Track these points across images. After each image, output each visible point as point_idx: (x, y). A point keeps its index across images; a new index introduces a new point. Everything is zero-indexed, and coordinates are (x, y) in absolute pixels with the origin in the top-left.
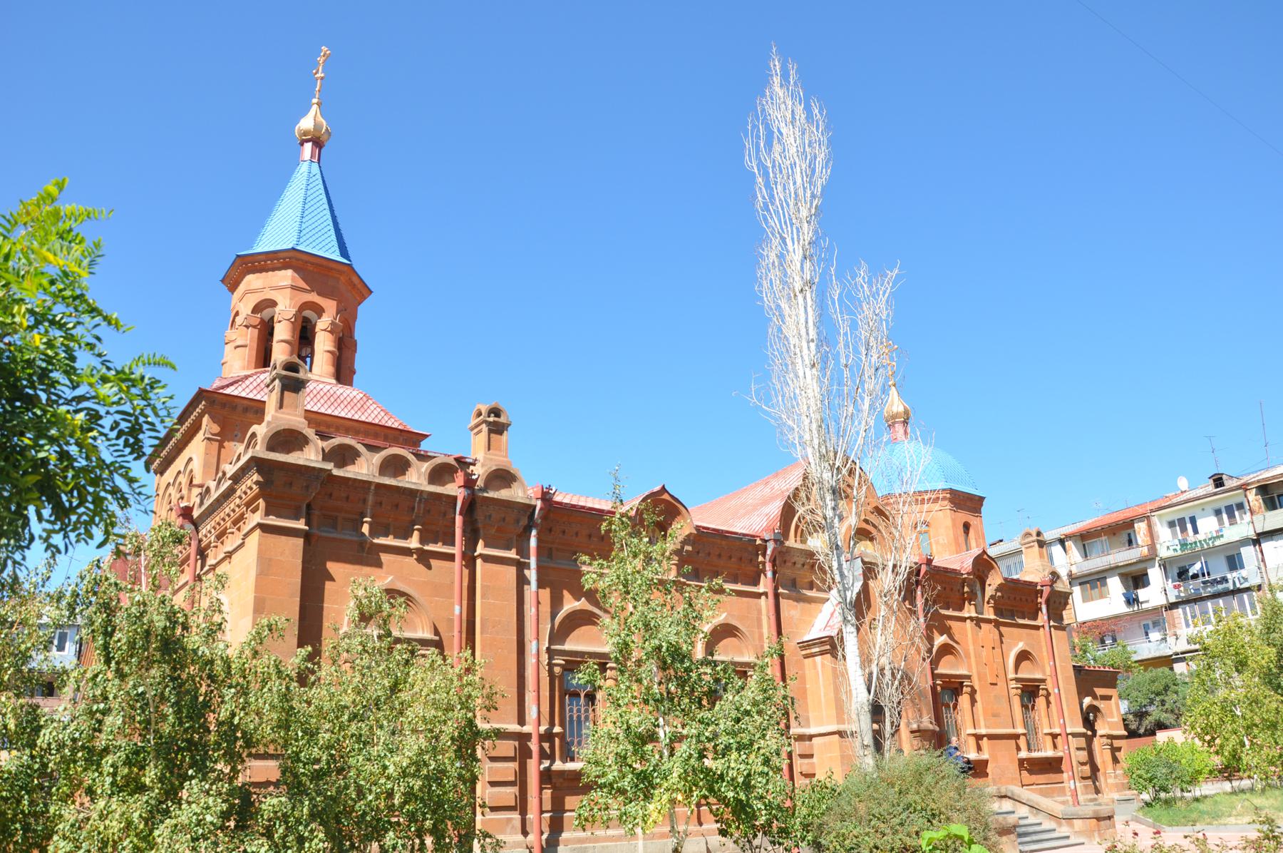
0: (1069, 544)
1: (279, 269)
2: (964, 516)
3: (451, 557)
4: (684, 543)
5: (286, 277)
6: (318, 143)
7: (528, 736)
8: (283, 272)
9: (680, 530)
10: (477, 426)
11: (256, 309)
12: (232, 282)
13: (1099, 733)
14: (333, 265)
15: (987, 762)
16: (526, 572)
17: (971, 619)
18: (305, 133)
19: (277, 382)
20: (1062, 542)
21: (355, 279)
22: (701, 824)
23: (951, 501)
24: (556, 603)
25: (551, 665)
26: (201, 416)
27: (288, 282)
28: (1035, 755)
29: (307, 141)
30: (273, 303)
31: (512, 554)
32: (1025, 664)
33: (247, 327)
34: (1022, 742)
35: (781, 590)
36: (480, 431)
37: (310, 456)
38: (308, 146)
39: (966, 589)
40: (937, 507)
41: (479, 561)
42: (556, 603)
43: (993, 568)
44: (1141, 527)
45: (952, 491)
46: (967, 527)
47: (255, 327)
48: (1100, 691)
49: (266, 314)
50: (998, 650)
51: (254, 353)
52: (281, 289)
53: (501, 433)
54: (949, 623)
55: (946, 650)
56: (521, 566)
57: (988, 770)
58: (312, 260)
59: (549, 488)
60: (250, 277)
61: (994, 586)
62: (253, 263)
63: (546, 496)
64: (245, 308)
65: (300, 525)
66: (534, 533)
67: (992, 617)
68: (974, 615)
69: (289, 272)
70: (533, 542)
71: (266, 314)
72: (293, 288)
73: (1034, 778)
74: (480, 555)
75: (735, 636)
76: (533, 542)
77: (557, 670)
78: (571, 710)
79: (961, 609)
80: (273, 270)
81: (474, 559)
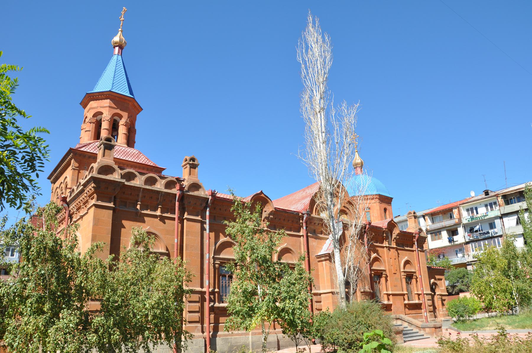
0: (426, 217)
1: (104, 99)
2: (384, 205)
3: (174, 219)
4: (270, 214)
5: (107, 102)
6: (121, 47)
7: (205, 293)
8: (106, 101)
9: (268, 210)
10: (185, 165)
11: (94, 116)
12: (84, 104)
13: (437, 293)
14: (126, 98)
15: (391, 305)
16: (205, 225)
17: (386, 247)
18: (116, 43)
19: (102, 145)
20: (424, 216)
21: (136, 104)
22: (275, 329)
23: (379, 199)
24: (217, 238)
25: (214, 264)
26: (71, 159)
27: (108, 105)
28: (411, 302)
29: (117, 46)
30: (101, 113)
31: (199, 218)
32: (408, 266)
33: (90, 123)
34: (406, 297)
35: (309, 234)
36: (186, 167)
37: (116, 177)
38: (117, 48)
39: (385, 235)
40: (373, 201)
41: (185, 221)
42: (217, 238)
43: (395, 226)
44: (455, 211)
45: (380, 195)
46: (385, 210)
47: (94, 123)
48: (437, 277)
49: (98, 118)
50: (397, 260)
51: (93, 134)
52: (105, 108)
53: (195, 168)
54: (378, 248)
55: (376, 259)
56: (203, 223)
57: (392, 308)
58: (118, 95)
59: (215, 191)
60: (92, 103)
61: (268, 212)
62: (93, 96)
63: (213, 194)
64: (90, 115)
65: (111, 205)
66: (208, 209)
67: (395, 246)
68: (388, 245)
69: (108, 101)
70: (208, 213)
71: (98, 118)
72: (110, 107)
73: (411, 311)
74: (186, 218)
75: (290, 253)
76: (208, 213)
77: (217, 266)
78: (222, 282)
79: (382, 243)
80: (102, 99)
81: (183, 220)
